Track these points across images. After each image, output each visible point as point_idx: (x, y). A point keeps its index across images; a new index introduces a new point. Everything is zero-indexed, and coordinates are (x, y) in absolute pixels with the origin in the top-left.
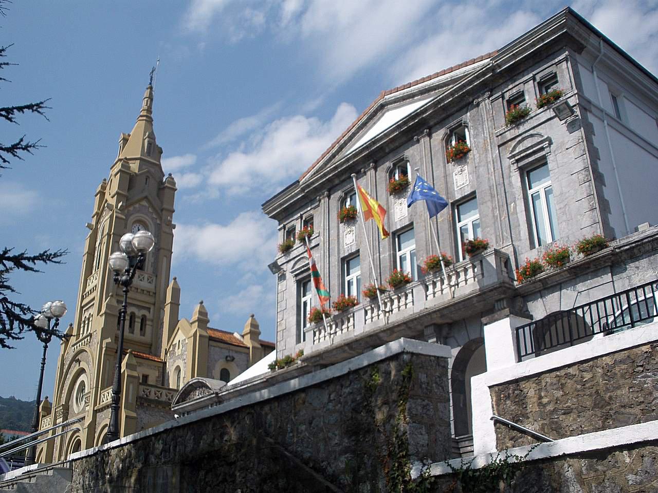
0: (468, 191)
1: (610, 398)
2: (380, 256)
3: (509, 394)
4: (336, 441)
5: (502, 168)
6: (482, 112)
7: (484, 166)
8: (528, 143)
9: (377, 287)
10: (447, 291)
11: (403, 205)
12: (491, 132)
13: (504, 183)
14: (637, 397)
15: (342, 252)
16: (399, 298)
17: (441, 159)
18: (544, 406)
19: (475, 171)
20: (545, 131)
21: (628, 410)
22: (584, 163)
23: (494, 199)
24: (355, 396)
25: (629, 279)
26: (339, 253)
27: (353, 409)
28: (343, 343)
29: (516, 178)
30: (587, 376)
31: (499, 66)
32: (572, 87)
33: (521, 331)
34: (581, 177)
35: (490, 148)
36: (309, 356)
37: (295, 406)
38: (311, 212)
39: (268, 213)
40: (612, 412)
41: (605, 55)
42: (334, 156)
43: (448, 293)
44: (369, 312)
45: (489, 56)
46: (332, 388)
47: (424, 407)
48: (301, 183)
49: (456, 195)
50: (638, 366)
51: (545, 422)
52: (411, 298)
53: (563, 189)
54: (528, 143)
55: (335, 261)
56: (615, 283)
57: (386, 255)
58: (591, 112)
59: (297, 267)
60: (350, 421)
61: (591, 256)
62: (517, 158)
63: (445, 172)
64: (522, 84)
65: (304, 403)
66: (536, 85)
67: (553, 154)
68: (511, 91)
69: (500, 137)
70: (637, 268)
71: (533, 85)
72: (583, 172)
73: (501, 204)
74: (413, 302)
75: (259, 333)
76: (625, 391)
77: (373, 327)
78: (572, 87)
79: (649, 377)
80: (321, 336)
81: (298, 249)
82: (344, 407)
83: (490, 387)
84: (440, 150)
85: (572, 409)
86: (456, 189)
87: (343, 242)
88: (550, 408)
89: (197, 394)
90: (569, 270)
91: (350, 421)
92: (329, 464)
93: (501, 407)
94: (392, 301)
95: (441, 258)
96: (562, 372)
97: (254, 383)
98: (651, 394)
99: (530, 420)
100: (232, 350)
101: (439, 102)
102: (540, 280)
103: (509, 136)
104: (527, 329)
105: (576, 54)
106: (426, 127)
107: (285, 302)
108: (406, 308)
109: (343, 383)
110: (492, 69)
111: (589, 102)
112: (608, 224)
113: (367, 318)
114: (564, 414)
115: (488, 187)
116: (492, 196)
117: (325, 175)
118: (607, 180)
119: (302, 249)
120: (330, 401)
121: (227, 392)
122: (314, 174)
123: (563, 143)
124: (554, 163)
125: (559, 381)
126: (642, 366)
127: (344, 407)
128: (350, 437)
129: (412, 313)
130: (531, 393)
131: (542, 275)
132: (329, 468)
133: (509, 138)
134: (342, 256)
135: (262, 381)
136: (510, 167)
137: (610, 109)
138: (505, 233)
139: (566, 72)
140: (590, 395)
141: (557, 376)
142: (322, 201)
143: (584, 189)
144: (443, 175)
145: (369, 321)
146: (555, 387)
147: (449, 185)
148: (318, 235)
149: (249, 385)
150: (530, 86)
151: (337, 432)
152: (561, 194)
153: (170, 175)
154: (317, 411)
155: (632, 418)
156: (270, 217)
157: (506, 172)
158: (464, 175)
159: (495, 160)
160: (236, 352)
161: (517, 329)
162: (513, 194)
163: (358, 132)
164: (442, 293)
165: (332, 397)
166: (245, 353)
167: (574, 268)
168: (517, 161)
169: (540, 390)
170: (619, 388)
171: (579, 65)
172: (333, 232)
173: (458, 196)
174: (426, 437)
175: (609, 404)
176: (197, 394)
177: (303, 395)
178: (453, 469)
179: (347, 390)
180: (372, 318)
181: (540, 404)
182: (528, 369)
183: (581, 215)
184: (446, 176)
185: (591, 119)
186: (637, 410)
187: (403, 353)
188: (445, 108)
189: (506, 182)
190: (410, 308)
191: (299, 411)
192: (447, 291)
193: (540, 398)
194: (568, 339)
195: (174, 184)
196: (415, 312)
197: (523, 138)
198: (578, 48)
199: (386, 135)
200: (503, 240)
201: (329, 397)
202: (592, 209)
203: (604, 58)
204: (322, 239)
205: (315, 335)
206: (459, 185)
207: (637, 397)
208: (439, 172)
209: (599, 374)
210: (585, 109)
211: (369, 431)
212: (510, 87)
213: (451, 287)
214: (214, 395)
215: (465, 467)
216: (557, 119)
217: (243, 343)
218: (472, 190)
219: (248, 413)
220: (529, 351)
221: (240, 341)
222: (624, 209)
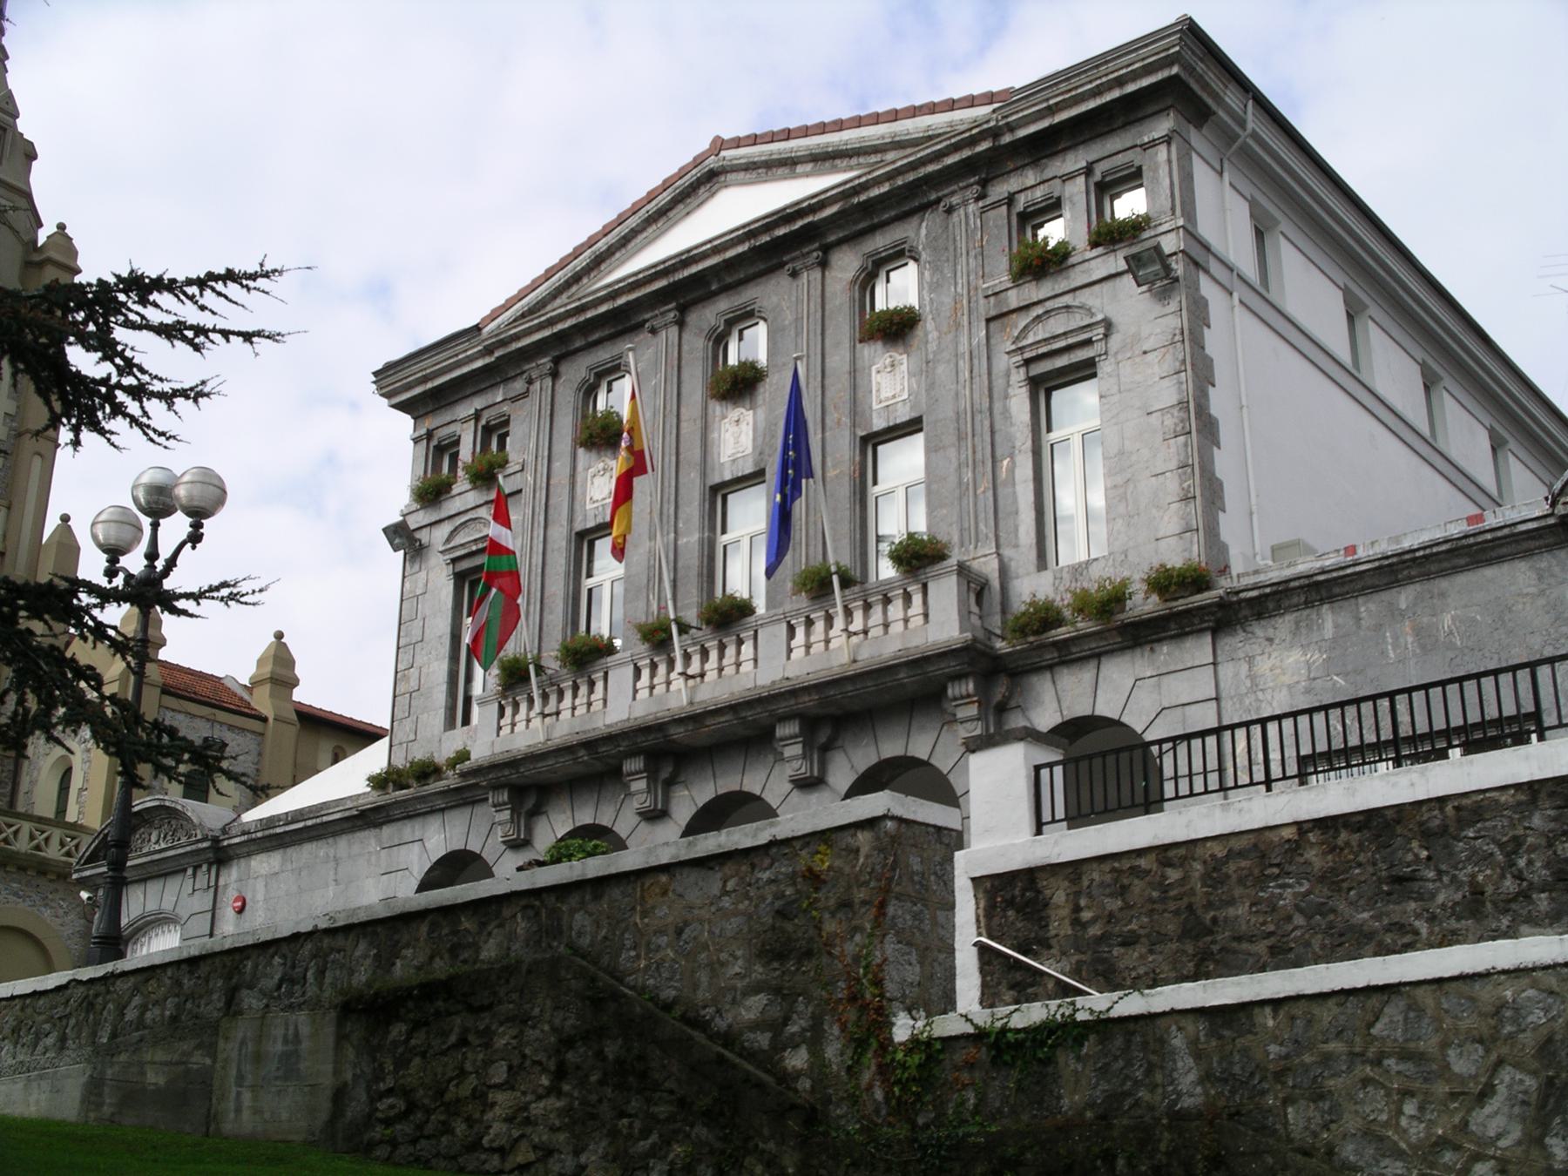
0: (903, 415)
1: (1214, 920)
2: (676, 540)
3: (1013, 897)
4: (737, 970)
5: (990, 374)
6: (957, 232)
7: (949, 361)
8: (1057, 325)
9: (672, 616)
10: (838, 640)
11: (743, 426)
12: (973, 284)
13: (991, 409)
14: (1264, 924)
15: (579, 518)
16: (722, 648)
17: (847, 328)
18: (1084, 926)
19: (926, 370)
20: (1100, 302)
21: (1245, 946)
22: (1180, 391)
23: (963, 444)
24: (782, 887)
25: (1250, 663)
26: (571, 520)
27: (778, 912)
28: (575, 739)
29: (1019, 403)
30: (1173, 875)
31: (1011, 128)
32: (1173, 209)
33: (1045, 773)
34: (1170, 422)
35: (966, 323)
36: (486, 764)
37: (643, 897)
38: (505, 408)
39: (387, 396)
40: (1215, 948)
41: (1255, 135)
42: (576, 278)
43: (840, 648)
44: (645, 673)
45: (989, 98)
46: (729, 868)
47: (915, 916)
48: (486, 330)
49: (875, 421)
50: (1272, 865)
51: (1084, 957)
52: (751, 650)
53: (1127, 443)
54: (1057, 325)
55: (560, 536)
56: (1220, 667)
57: (691, 539)
58: (1207, 272)
59: (460, 539)
60: (769, 934)
61: (1175, 604)
62: (1027, 355)
63: (854, 361)
64: (1058, 181)
65: (665, 893)
66: (1092, 188)
67: (1111, 359)
68: (1025, 184)
69: (992, 299)
70: (1270, 640)
71: (1083, 188)
72: (1175, 412)
73: (979, 456)
74: (756, 660)
75: (295, 683)
76: (1241, 910)
77: (654, 710)
78: (1173, 209)
79: (1289, 886)
80: (517, 718)
81: (464, 497)
82: (756, 906)
83: (973, 879)
84: (846, 308)
85: (1139, 936)
86: (875, 406)
87: (584, 494)
88: (1095, 931)
89: (154, 839)
90: (1117, 625)
91: (769, 934)
92: (718, 1011)
93: (996, 921)
94: (705, 654)
95: (833, 569)
96: (1126, 864)
97: (325, 819)
98: (1289, 918)
99: (1053, 951)
100: (221, 724)
101: (857, 190)
102: (1055, 644)
103: (1014, 299)
104: (1058, 770)
105: (1192, 128)
106: (816, 245)
107: (418, 623)
108: (738, 671)
109: (756, 861)
110: (995, 133)
111: (1206, 248)
112: (1217, 535)
113: (639, 685)
114: (1123, 944)
115: (951, 414)
116: (961, 437)
117: (551, 322)
118: (1225, 433)
119: (473, 498)
120: (725, 893)
121: (245, 838)
122: (523, 316)
123: (1137, 338)
124: (1113, 380)
125: (1116, 881)
126: (1278, 865)
127: (756, 906)
128: (769, 963)
129: (751, 685)
130: (1060, 897)
131: (1061, 633)
132: (717, 1019)
133: (1014, 304)
134: (578, 527)
135: (347, 814)
136: (1008, 375)
137: (1247, 263)
138: (982, 526)
139: (1163, 172)
140: (1177, 913)
141: (1113, 870)
142: (537, 385)
143: (1173, 450)
144: (847, 368)
145: (643, 694)
146: (1108, 891)
147: (860, 394)
148: (518, 467)
149: (309, 823)
150: (1076, 190)
151: (739, 953)
152: (1121, 453)
153: (61, 227)
154: (696, 912)
155: (1251, 960)
156: (394, 406)
157: (999, 383)
158: (898, 377)
159: (975, 353)
160: (231, 727)
161: (1037, 769)
162: (1010, 438)
163: (644, 229)
164: (827, 648)
165: (730, 885)
166: (253, 732)
167: (1132, 624)
168: (1027, 362)
169: (1078, 894)
170: (1231, 902)
171: (1194, 156)
172: (561, 467)
173: (878, 424)
174: (918, 969)
175: (1211, 932)
176: (154, 839)
177: (664, 878)
178: (976, 1027)
179: (765, 876)
180: (652, 687)
181: (1076, 922)
182: (1056, 850)
183: (1158, 507)
184: (854, 372)
185: (1207, 288)
186: (1261, 948)
187: (885, 817)
188: (869, 207)
189: (997, 406)
190: (747, 674)
191: (653, 908)
192: (838, 640)
193: (1077, 909)
194: (1139, 799)
195: (74, 253)
196: (759, 683)
197: (1047, 312)
198: (1198, 113)
199: (716, 250)
200: (977, 541)
201: (724, 885)
202: (1187, 498)
203: (1250, 142)
204: (530, 479)
205: (501, 714)
206: (883, 395)
207: (1264, 924)
208: (838, 360)
209: (1197, 874)
210: (1197, 264)
211: (809, 954)
212: (1030, 181)
213: (850, 634)
214: (205, 845)
215: (998, 1024)
216: (1128, 280)
217: (248, 705)
218: (914, 415)
219: (525, 907)
220: (1060, 814)
221: (241, 699)
222: (1254, 500)
